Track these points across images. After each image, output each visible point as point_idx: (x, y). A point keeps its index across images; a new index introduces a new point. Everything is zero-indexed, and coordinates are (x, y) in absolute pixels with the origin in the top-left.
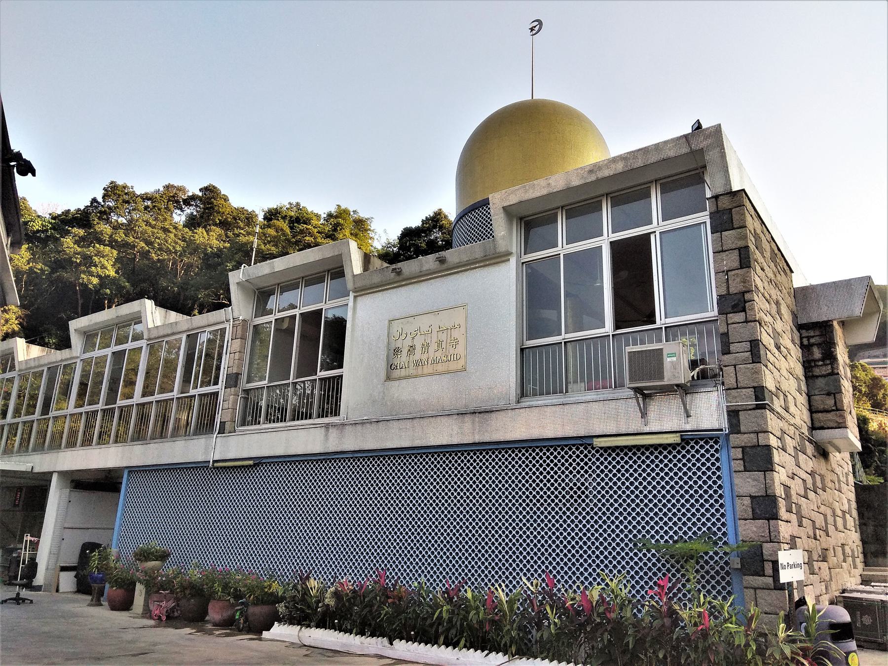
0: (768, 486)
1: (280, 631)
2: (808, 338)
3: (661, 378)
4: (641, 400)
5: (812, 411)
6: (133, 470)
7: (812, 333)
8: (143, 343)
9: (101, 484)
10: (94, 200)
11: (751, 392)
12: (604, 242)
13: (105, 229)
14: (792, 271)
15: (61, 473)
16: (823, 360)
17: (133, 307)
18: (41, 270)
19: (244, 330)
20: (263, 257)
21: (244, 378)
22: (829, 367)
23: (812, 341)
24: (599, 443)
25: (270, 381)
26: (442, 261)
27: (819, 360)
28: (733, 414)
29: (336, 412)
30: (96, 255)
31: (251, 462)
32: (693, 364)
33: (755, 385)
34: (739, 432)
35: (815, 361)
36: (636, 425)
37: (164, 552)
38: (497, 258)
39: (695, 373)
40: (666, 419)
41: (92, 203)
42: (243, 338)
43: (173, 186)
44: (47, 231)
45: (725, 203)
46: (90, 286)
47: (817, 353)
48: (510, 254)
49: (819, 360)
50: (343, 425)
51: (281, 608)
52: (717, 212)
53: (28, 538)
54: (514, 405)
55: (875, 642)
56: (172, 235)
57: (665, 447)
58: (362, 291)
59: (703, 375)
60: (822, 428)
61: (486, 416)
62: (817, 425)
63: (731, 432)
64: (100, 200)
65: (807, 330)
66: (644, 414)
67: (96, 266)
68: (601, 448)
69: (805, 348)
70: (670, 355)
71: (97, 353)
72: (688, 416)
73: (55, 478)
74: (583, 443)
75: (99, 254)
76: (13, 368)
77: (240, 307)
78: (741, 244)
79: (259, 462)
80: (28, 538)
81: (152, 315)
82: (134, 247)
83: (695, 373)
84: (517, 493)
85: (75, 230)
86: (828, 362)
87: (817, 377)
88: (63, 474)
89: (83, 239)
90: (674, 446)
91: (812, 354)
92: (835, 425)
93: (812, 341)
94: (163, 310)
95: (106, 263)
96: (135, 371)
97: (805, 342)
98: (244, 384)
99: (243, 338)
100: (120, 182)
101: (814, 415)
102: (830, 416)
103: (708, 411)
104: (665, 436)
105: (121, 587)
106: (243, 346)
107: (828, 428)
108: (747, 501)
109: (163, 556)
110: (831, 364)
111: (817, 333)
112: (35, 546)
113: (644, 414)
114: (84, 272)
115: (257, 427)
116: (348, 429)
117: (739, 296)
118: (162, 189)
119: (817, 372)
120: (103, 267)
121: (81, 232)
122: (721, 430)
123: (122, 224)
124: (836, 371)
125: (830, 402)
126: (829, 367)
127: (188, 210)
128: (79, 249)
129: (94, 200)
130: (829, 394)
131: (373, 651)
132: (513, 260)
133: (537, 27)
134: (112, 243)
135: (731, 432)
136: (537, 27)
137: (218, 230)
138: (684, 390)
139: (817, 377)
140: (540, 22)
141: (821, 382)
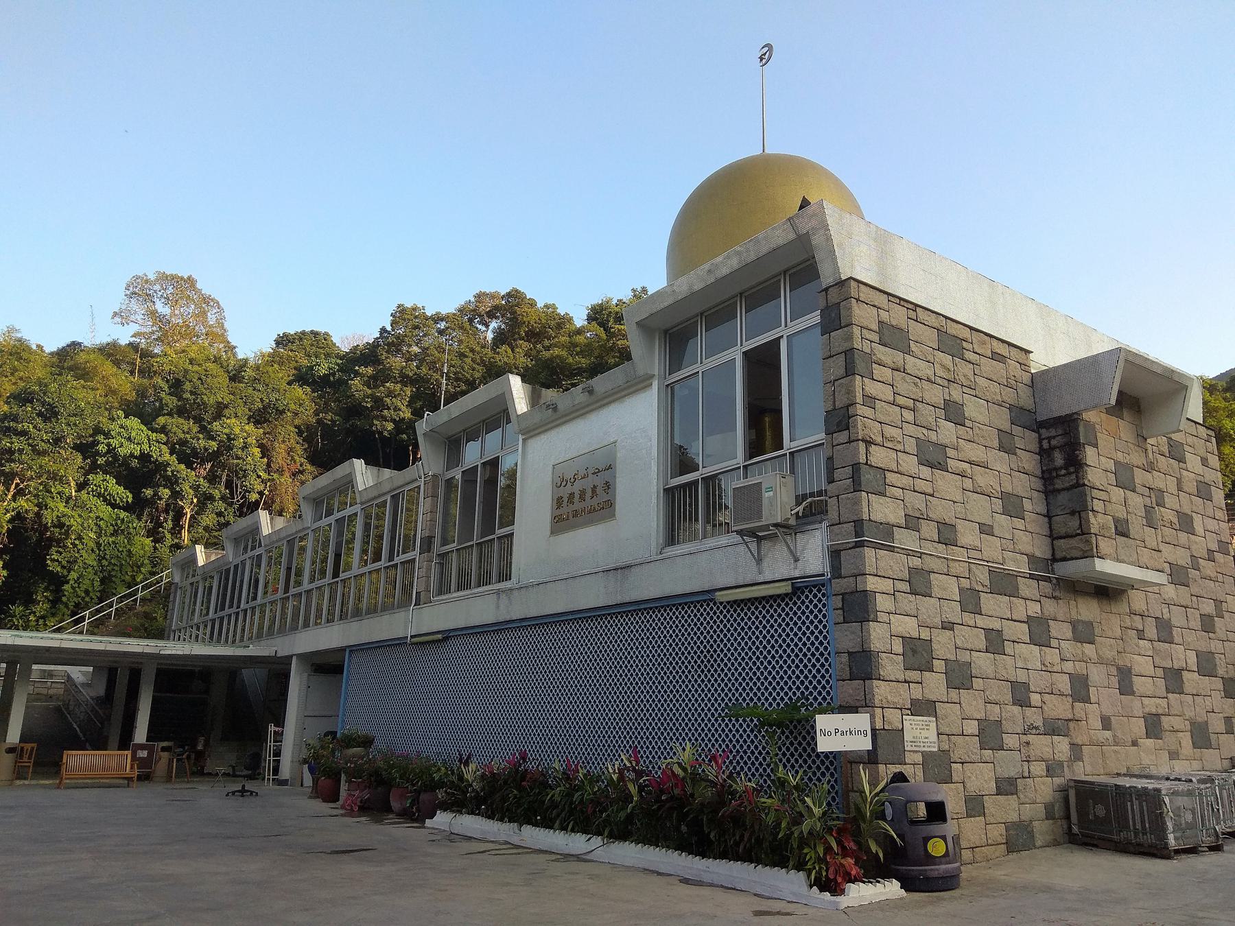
0: (864, 640)
1: (442, 819)
2: (1049, 439)
3: (759, 516)
4: (753, 547)
5: (1053, 537)
6: (355, 649)
7: (1053, 432)
8: (357, 508)
9: (327, 666)
10: (383, 330)
11: (850, 526)
12: (736, 355)
13: (396, 362)
14: (1028, 352)
15: (300, 656)
16: (1066, 467)
17: (340, 471)
18: (332, 420)
19: (435, 487)
20: (451, 398)
21: (437, 541)
22: (1074, 476)
23: (1054, 442)
24: (722, 596)
25: (459, 543)
26: (591, 392)
27: (1061, 468)
28: (835, 554)
29: (505, 575)
30: (387, 396)
31: (440, 636)
32: (799, 499)
33: (856, 518)
34: (840, 577)
35: (1056, 469)
36: (749, 573)
37: (366, 737)
38: (638, 384)
39: (800, 508)
40: (779, 566)
41: (381, 334)
42: (435, 496)
43: (485, 294)
44: (334, 374)
45: (834, 296)
46: (386, 433)
47: (1059, 459)
48: (653, 376)
49: (1061, 468)
50: (511, 590)
51: (440, 794)
52: (827, 307)
53: (272, 728)
54: (654, 557)
55: (1111, 840)
56: (468, 360)
57: (774, 598)
58: (531, 431)
59: (812, 511)
60: (1064, 559)
61: (626, 571)
62: (1059, 555)
63: (834, 577)
64: (389, 328)
65: (1047, 429)
66: (759, 561)
67: (389, 409)
68: (728, 602)
69: (1044, 453)
70: (770, 489)
71: (325, 521)
72: (796, 560)
73: (294, 659)
74: (702, 599)
75: (390, 394)
76: (260, 545)
77: (429, 462)
78: (846, 346)
79: (447, 636)
80: (272, 728)
81: (362, 473)
82: (428, 381)
83: (800, 508)
84: (818, 660)
85: (362, 370)
86: (1072, 469)
87: (1059, 491)
88: (304, 657)
89: (374, 378)
90: (782, 597)
91: (1052, 460)
92: (1079, 554)
93: (1054, 442)
94: (375, 469)
95: (399, 404)
96: (381, 537)
97: (1045, 445)
98: (437, 547)
99: (435, 496)
100: (409, 305)
101: (1058, 543)
102: (1073, 542)
103: (812, 553)
104: (777, 584)
105: (329, 777)
106: (434, 505)
107: (1072, 559)
108: (845, 658)
109: (367, 742)
110: (1077, 472)
111: (1060, 432)
112: (279, 736)
113: (759, 561)
114: (377, 417)
115: (468, 592)
116: (516, 593)
117: (843, 411)
118: (473, 299)
119: (1059, 484)
120: (397, 409)
121: (370, 370)
122: (823, 575)
123: (416, 355)
124: (1081, 482)
125: (1074, 523)
126: (1074, 476)
127: (494, 324)
128: (369, 392)
129: (383, 330)
130: (1073, 513)
131: (503, 838)
132: (655, 384)
133: (766, 55)
134: (405, 380)
135: (834, 577)
136: (766, 55)
137: (525, 345)
138: (789, 529)
139: (1059, 491)
140: (769, 46)
141: (1063, 498)
